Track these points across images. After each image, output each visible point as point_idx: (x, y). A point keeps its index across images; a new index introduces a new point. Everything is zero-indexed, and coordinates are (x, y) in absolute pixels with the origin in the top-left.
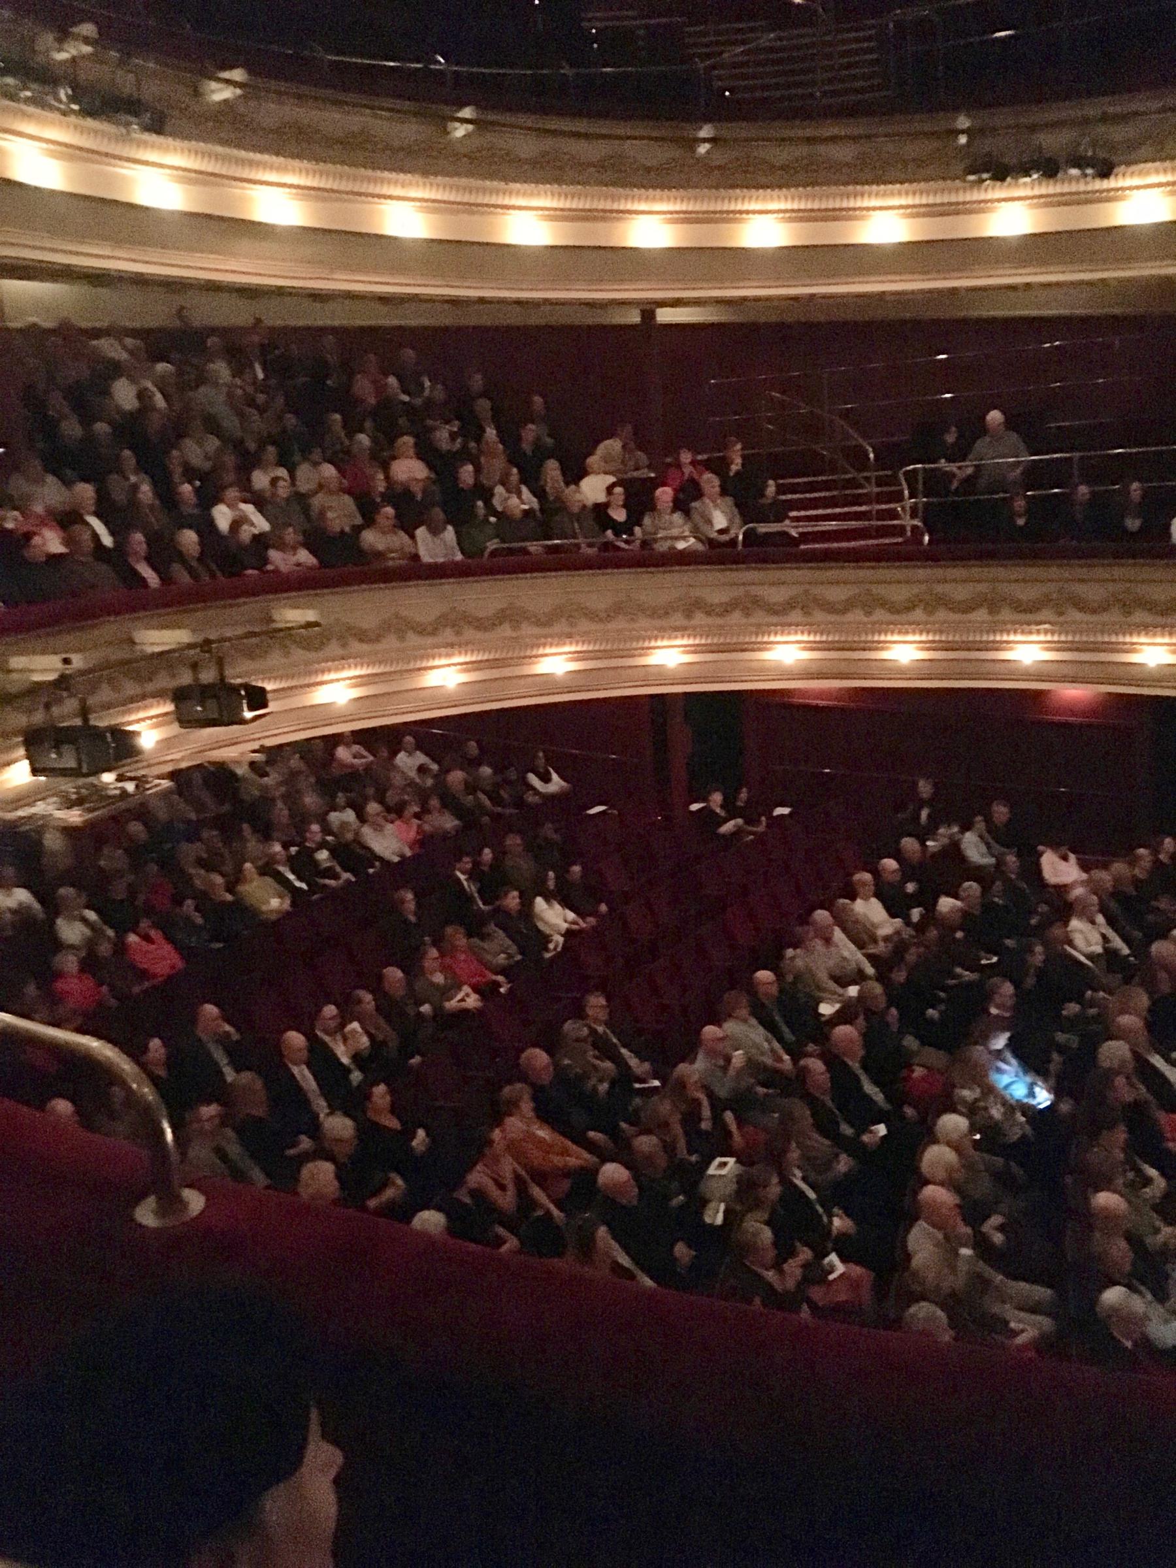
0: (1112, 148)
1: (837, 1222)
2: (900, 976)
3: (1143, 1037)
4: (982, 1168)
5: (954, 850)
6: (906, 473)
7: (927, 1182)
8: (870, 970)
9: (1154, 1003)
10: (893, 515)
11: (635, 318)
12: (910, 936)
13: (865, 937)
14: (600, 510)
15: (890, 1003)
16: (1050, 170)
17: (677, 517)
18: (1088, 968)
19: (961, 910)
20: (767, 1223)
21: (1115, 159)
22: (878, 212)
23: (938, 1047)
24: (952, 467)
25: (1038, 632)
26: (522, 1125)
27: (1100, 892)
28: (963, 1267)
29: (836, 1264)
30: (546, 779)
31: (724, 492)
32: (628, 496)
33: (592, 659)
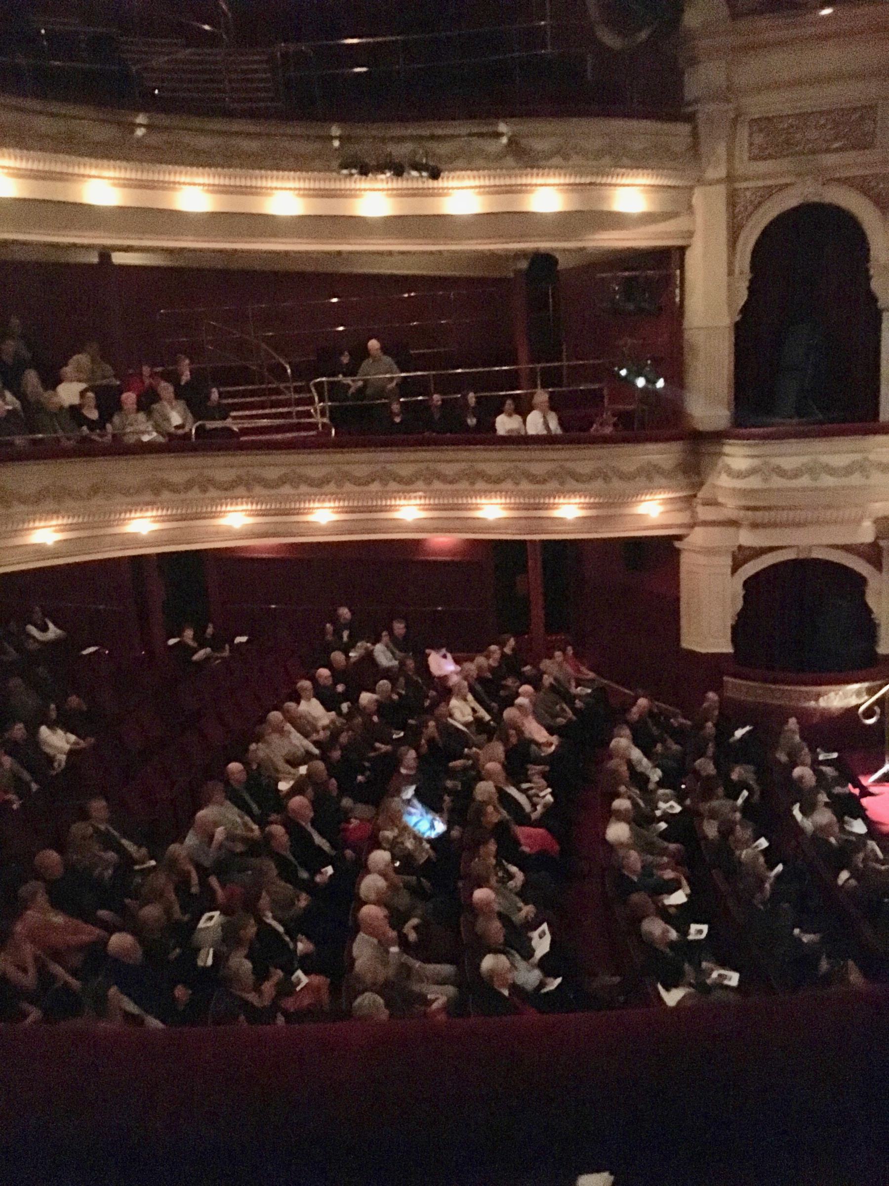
0: (440, 158)
1: (300, 946)
2: (336, 754)
3: (502, 777)
4: (401, 884)
5: (369, 657)
6: (316, 385)
7: (365, 903)
8: (316, 751)
9: (507, 753)
10: (308, 415)
11: (94, 259)
12: (342, 723)
13: (309, 728)
14: (75, 411)
15: (330, 776)
16: (399, 171)
17: (141, 416)
18: (462, 731)
19: (377, 701)
20: (247, 957)
21: (442, 166)
22: (368, 192)
23: (366, 803)
24: (348, 380)
25: (415, 498)
26: (42, 916)
27: (470, 679)
28: (392, 960)
29: (301, 977)
30: (44, 629)
31: (177, 396)
32: (97, 398)
33: (77, 530)
